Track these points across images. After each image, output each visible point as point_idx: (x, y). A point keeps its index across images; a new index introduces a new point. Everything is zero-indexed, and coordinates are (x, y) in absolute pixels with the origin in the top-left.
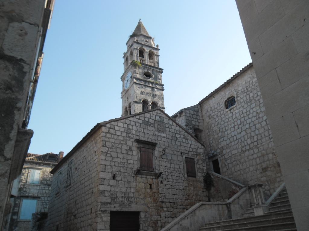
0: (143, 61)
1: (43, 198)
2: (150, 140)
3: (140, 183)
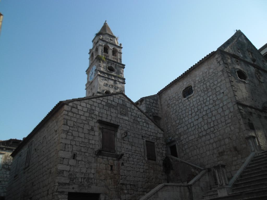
0: (107, 57)
1: (3, 182)
2: (112, 122)
3: (101, 164)
